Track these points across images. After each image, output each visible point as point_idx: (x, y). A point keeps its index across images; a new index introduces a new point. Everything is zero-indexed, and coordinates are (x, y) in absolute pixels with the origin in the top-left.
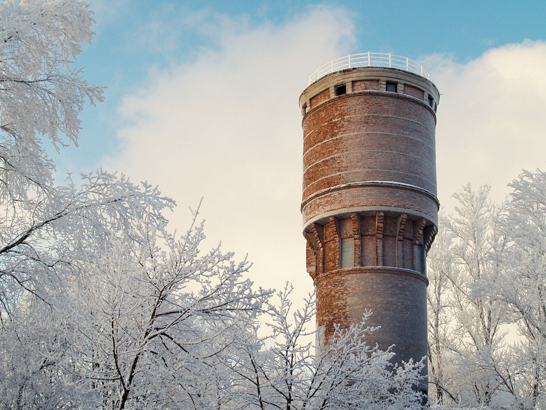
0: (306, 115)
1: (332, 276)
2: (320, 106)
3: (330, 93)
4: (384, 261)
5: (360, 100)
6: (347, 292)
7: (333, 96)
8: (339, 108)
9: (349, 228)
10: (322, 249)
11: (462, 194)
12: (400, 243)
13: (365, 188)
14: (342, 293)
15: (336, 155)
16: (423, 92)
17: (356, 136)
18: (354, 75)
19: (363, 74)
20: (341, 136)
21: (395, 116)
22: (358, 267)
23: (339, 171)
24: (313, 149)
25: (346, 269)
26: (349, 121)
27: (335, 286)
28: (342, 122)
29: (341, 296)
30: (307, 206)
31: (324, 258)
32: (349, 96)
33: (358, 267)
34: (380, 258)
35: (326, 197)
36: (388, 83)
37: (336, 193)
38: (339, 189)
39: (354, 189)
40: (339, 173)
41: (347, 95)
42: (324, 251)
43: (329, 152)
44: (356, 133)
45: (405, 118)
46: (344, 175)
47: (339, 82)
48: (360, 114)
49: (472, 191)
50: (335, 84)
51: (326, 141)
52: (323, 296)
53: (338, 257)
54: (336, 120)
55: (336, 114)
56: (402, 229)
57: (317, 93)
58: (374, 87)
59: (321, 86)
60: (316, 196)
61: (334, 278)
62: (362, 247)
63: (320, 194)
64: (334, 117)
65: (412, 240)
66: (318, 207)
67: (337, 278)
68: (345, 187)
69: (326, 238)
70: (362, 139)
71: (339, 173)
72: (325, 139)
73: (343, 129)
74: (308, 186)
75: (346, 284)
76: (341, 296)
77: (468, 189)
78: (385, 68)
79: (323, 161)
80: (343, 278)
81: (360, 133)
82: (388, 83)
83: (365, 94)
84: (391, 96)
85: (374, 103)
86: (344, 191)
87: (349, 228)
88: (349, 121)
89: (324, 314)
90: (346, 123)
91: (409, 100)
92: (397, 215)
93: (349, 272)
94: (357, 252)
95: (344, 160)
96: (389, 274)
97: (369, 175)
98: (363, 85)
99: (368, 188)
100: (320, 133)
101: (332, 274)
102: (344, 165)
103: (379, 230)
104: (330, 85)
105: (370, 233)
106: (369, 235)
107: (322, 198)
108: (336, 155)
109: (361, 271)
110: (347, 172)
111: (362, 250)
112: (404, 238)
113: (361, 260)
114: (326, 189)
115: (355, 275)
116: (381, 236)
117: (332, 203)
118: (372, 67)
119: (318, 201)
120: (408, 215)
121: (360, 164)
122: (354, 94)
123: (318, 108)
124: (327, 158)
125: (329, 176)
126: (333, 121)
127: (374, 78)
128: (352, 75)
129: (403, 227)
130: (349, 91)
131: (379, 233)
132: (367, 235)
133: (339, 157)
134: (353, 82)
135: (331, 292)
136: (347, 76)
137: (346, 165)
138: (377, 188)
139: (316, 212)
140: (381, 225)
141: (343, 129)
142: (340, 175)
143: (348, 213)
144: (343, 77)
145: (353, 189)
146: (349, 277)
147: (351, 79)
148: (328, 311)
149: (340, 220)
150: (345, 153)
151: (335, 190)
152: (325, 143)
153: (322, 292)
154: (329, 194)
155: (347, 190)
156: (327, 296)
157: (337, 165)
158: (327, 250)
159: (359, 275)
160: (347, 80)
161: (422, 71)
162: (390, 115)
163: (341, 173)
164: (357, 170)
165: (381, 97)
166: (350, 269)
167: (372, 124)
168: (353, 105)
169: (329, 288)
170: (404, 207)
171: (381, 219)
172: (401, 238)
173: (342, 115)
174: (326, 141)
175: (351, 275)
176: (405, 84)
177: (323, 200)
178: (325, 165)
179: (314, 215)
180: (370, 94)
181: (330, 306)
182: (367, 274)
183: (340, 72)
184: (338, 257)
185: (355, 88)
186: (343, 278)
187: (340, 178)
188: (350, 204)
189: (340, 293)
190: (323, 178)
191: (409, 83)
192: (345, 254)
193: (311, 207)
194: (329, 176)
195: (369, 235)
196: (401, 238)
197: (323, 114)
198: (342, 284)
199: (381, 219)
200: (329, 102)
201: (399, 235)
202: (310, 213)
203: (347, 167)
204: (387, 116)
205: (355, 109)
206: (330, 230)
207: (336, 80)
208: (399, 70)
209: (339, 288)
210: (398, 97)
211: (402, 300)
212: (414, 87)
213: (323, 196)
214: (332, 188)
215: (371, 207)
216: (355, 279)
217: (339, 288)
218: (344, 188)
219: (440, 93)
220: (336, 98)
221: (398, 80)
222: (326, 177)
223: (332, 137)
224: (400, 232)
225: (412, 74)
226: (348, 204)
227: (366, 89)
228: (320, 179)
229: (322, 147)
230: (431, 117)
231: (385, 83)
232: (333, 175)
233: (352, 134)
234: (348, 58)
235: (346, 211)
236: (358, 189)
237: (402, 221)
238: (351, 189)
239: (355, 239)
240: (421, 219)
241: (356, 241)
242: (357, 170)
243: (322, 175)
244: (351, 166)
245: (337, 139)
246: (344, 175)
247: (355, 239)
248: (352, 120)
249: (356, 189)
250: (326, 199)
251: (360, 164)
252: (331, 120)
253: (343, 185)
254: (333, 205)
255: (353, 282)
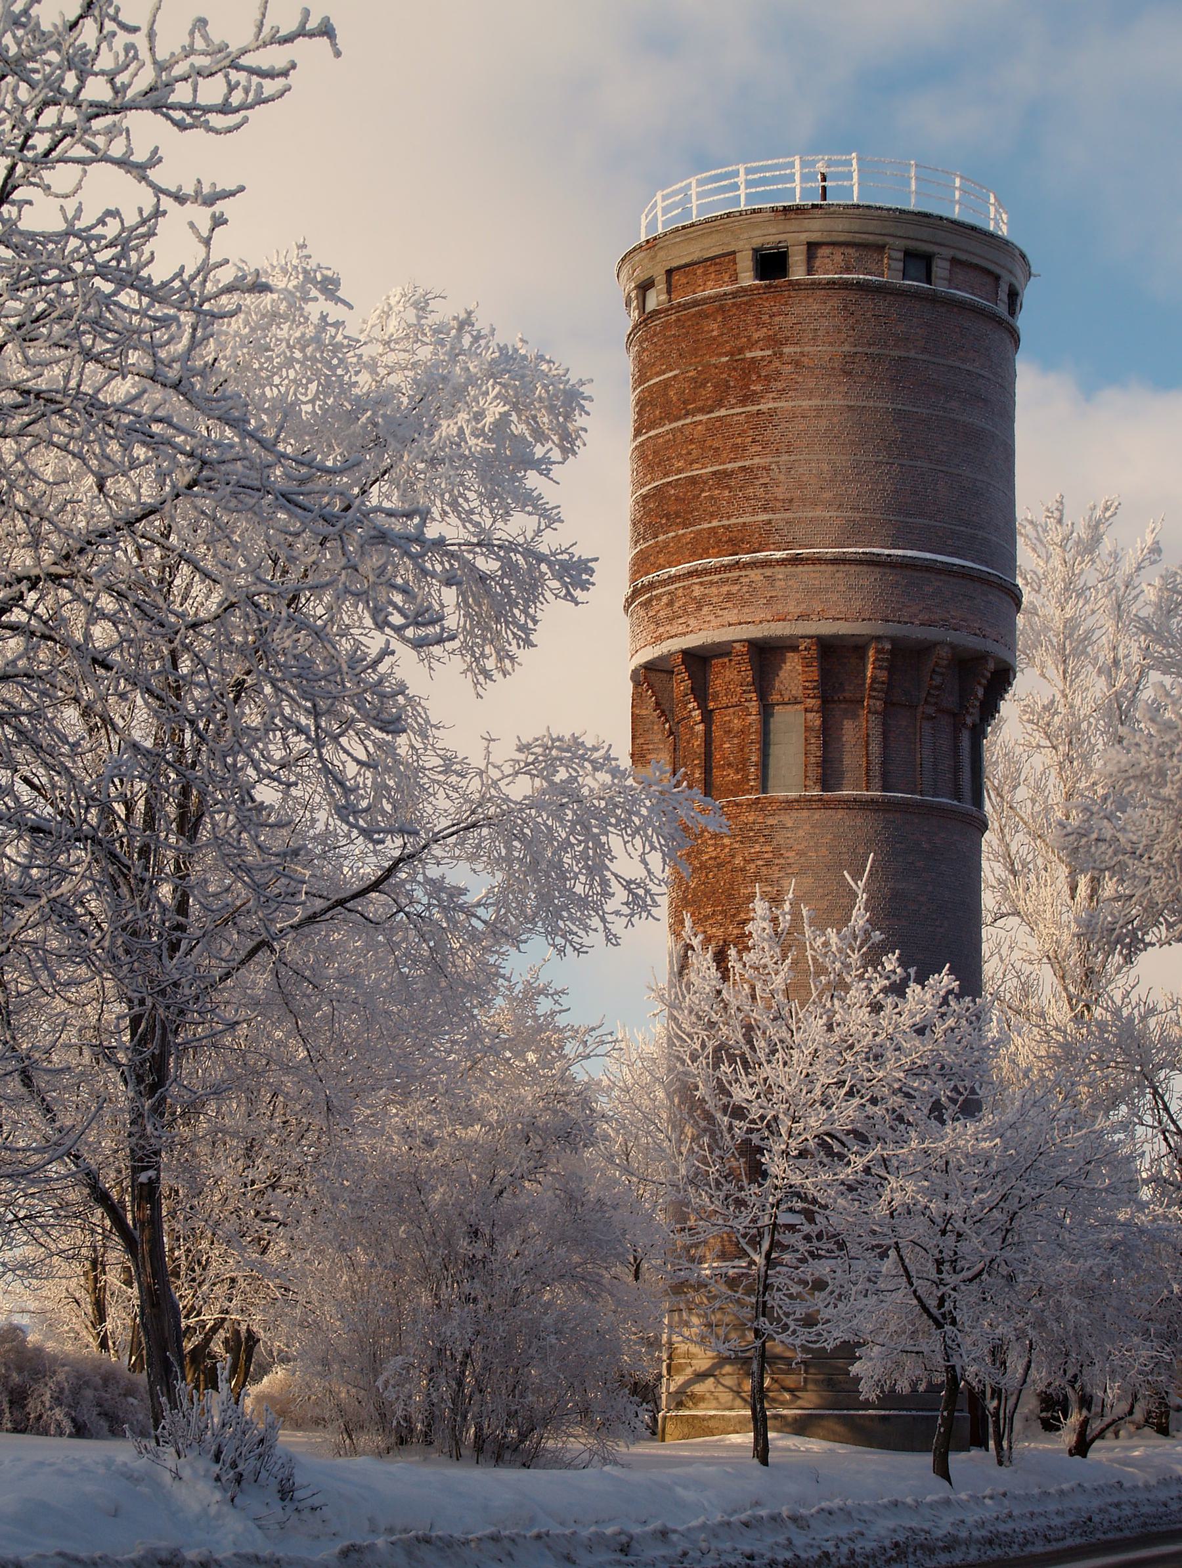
0: (647, 318)
1: (734, 810)
2: (704, 301)
3: (739, 267)
4: (885, 775)
5: (830, 304)
6: (782, 861)
7: (747, 279)
8: (765, 318)
9: (793, 675)
10: (701, 727)
11: (1031, 522)
12: (927, 727)
13: (842, 567)
14: (768, 863)
15: (757, 460)
16: (997, 278)
17: (818, 409)
18: (816, 224)
19: (840, 225)
20: (771, 405)
21: (925, 357)
22: (816, 793)
23: (765, 510)
24: (680, 430)
25: (778, 793)
26: (797, 364)
27: (745, 840)
28: (777, 364)
29: (764, 871)
30: (658, 598)
31: (708, 755)
32: (797, 285)
33: (816, 793)
34: (876, 769)
35: (724, 582)
36: (910, 255)
37: (755, 575)
38: (766, 563)
39: (811, 568)
40: (765, 517)
41: (791, 283)
42: (708, 733)
43: (735, 447)
44: (816, 402)
45: (950, 362)
46: (782, 524)
47: (771, 239)
48: (831, 344)
49: (1067, 520)
50: (757, 242)
51: (723, 412)
52: (703, 866)
53: (754, 759)
54: (759, 354)
55: (756, 336)
56: (937, 688)
57: (695, 257)
58: (868, 265)
59: (707, 242)
60: (690, 574)
61: (743, 818)
62: (828, 735)
63: (706, 572)
64: (752, 345)
65: (954, 715)
66: (699, 608)
67: (751, 819)
68: (784, 560)
69: (716, 697)
70: (835, 420)
71: (765, 517)
72: (720, 404)
73: (780, 385)
74: (661, 538)
75: (779, 839)
76: (764, 871)
77: (1057, 514)
78: (902, 212)
79: (714, 473)
80: (771, 821)
81: (830, 402)
82: (910, 255)
83: (846, 285)
84: (916, 295)
85: (869, 315)
86: (780, 572)
87: (793, 675)
88: (797, 364)
89: (707, 917)
90: (788, 368)
91: (962, 305)
92: (922, 650)
93: (789, 805)
94: (813, 748)
95: (782, 477)
96: (898, 815)
97: (853, 532)
98: (838, 258)
99: (853, 569)
100: (703, 385)
101: (737, 805)
102: (780, 492)
103: (875, 690)
104: (740, 245)
105: (847, 695)
106: (845, 701)
107: (711, 583)
108: (757, 460)
109: (825, 804)
110: (788, 515)
111: (825, 745)
112: (939, 711)
113: (828, 773)
114: (727, 560)
115: (805, 813)
116: (879, 705)
117: (745, 603)
118: (869, 207)
119: (697, 591)
120: (953, 647)
121: (827, 495)
122: (813, 283)
123: (696, 303)
124: (729, 466)
125: (733, 521)
126: (749, 355)
127: (871, 238)
128: (807, 224)
129: (938, 680)
130: (798, 272)
131: (874, 697)
132: (840, 701)
133: (767, 469)
134: (812, 247)
135: (733, 856)
136: (793, 225)
137: (788, 496)
138: (877, 570)
139: (692, 622)
140: (883, 675)
141: (780, 385)
142: (769, 522)
143: (790, 637)
144: (781, 227)
145: (806, 568)
146: (788, 819)
147: (804, 237)
148: (723, 912)
149: (765, 655)
150: (785, 457)
151: (753, 565)
152: (719, 419)
153: (700, 852)
154: (736, 574)
155: (790, 569)
156: (719, 866)
157: (760, 492)
158: (717, 733)
159: (817, 815)
160: (794, 239)
161: (992, 209)
162: (912, 354)
163: (771, 516)
164: (818, 513)
165: (889, 298)
166: (793, 795)
167: (864, 379)
168: (810, 315)
169: (724, 846)
170: (945, 624)
171: (882, 660)
172: (930, 710)
173: (774, 342)
174: (723, 412)
175: (794, 814)
176: (955, 261)
177: (714, 590)
178: (719, 485)
179: (681, 629)
180: (861, 286)
181: (730, 897)
182: (840, 814)
183: (773, 210)
184: (754, 759)
185: (817, 263)
186: (771, 821)
187: (768, 532)
188: (798, 610)
189: (760, 863)
190: (715, 523)
191: (963, 256)
192: (774, 750)
193: (670, 603)
194: (733, 521)
195: (845, 701)
196: (930, 710)
197: (714, 328)
198: (769, 839)
199: (882, 660)
200: (734, 294)
201: (926, 702)
202: (670, 620)
203: (791, 501)
204: (903, 354)
205: (813, 331)
206: (730, 674)
207: (757, 232)
208: (941, 218)
209: (757, 848)
210: (933, 299)
211: (930, 888)
212: (976, 267)
213: (716, 578)
214: (746, 558)
215: (859, 623)
216: (807, 827)
217: (757, 848)
218: (782, 562)
219: (1033, 271)
220: (758, 287)
221: (935, 249)
222: (725, 522)
223: (744, 401)
224: (929, 693)
225: (973, 228)
226: (793, 609)
227: (848, 270)
228: (706, 526)
229: (713, 428)
230: (1010, 347)
231: (900, 255)
232: (747, 519)
233: (805, 404)
234: (792, 165)
235: (787, 632)
236: (823, 567)
237: (937, 664)
238: (800, 568)
239: (806, 710)
240: (983, 657)
241: (810, 716)
242: (818, 513)
243: (712, 515)
244: (803, 500)
245: (759, 412)
246: (782, 524)
247: (806, 710)
248: (805, 360)
249: (818, 568)
250: (725, 589)
251: (827, 495)
252: (741, 351)
253: (779, 555)
254: (746, 610)
255: (801, 833)
